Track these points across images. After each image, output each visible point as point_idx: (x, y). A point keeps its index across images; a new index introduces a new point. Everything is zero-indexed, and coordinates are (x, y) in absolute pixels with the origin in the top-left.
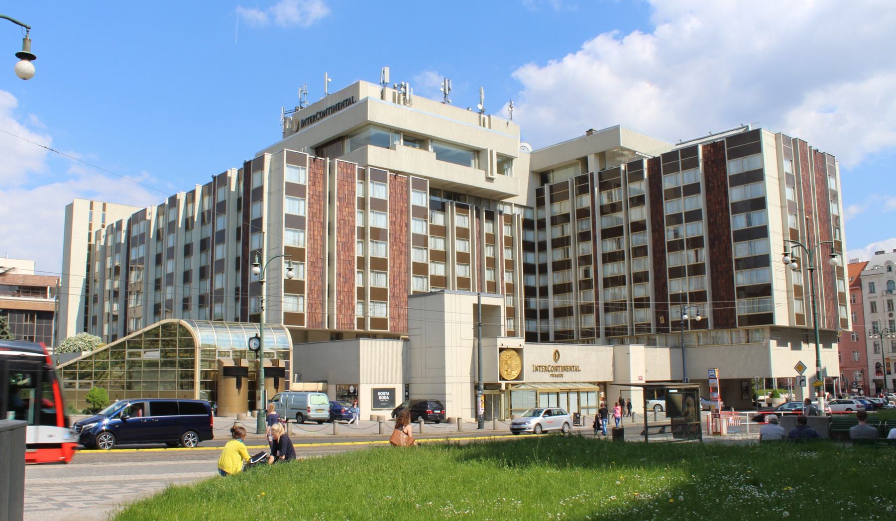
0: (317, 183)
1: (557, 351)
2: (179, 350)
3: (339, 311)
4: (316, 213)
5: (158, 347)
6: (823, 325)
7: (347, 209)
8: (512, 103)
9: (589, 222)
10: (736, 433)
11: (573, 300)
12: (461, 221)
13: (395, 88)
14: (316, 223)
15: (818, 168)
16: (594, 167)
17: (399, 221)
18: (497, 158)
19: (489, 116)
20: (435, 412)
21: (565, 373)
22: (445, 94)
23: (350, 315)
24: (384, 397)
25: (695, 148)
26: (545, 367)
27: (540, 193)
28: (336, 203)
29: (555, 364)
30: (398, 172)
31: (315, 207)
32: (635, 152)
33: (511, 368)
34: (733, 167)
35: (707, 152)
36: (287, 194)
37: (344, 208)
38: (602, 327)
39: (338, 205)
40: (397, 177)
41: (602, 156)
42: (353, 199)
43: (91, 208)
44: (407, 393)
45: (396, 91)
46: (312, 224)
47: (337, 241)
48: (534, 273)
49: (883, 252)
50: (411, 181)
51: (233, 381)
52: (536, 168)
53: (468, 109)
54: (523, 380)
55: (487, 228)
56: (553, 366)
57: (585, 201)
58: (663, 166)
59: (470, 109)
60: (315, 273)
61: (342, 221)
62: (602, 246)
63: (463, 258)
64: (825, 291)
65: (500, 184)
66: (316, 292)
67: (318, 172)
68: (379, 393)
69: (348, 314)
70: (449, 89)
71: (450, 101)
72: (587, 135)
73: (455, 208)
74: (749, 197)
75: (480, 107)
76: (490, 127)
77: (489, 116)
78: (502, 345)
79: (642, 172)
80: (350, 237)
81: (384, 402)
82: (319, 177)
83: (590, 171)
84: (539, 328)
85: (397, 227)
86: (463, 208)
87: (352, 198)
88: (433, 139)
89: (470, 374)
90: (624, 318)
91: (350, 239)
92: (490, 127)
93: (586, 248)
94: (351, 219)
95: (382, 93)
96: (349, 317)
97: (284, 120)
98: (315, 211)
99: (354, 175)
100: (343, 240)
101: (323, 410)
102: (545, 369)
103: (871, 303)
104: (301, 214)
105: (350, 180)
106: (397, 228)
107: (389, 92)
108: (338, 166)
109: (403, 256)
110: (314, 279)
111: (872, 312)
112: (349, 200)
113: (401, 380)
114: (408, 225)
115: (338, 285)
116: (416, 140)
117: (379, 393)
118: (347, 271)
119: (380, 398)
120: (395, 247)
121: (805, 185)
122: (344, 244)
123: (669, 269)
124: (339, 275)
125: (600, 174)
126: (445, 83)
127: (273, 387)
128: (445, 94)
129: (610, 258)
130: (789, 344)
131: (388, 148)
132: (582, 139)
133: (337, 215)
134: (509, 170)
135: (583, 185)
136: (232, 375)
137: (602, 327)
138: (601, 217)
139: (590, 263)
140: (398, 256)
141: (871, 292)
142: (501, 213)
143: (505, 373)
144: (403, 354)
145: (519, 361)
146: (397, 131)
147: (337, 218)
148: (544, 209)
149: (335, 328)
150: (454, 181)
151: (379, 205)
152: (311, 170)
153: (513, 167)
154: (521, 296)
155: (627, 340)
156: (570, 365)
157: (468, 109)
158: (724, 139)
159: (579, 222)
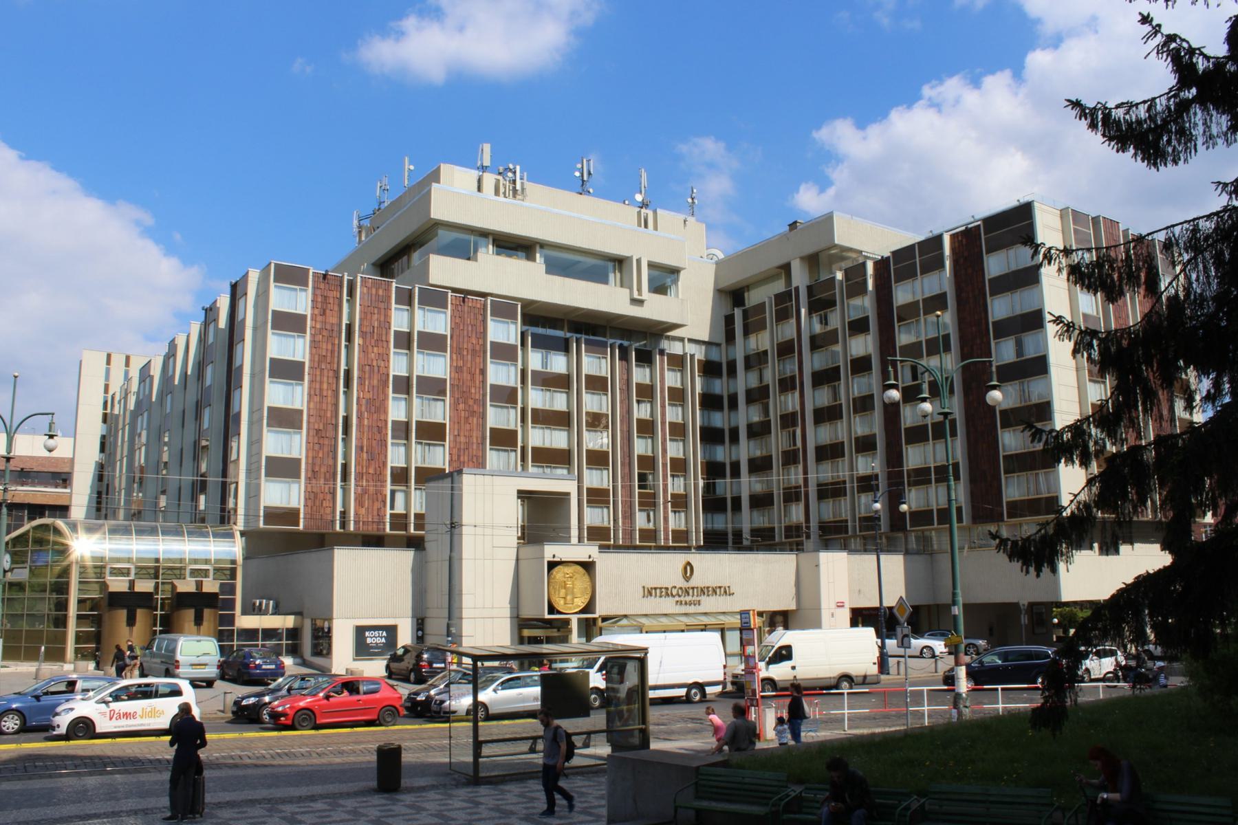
0: (328, 311)
1: (689, 564)
3: (359, 502)
4: (323, 356)
5: (27, 562)
7: (375, 349)
8: (695, 191)
9: (794, 362)
10: (811, 731)
11: (779, 479)
12: (593, 365)
13: (500, 174)
14: (325, 371)
16: (800, 278)
17: (469, 366)
18: (649, 269)
19: (655, 212)
20: (435, 665)
21: (703, 599)
22: (583, 181)
23: (379, 510)
24: (373, 639)
25: (938, 239)
26: (667, 589)
27: (729, 320)
28: (357, 340)
29: (684, 584)
31: (324, 347)
32: (862, 251)
33: (573, 593)
34: (995, 265)
35: (957, 245)
36: (273, 328)
37: (370, 348)
38: (814, 524)
39: (361, 343)
40: (466, 300)
41: (813, 261)
42: (387, 334)
43: (108, 362)
44: (420, 633)
45: (500, 178)
46: (318, 373)
47: (358, 398)
48: (722, 442)
50: (489, 306)
51: (123, 614)
52: (723, 285)
53: (624, 203)
54: (594, 613)
55: (640, 375)
56: (681, 588)
57: (788, 331)
58: (894, 269)
59: (627, 202)
60: (321, 446)
61: (367, 367)
63: (596, 421)
65: (655, 309)
66: (322, 476)
67: (331, 294)
68: (367, 634)
69: (375, 508)
70: (589, 174)
71: (591, 191)
72: (791, 230)
73: (583, 345)
74: (1018, 312)
75: (639, 198)
76: (656, 228)
77: (655, 212)
78: (554, 556)
79: (865, 282)
80: (381, 391)
81: (377, 646)
83: (794, 284)
84: (730, 526)
85: (465, 374)
86: (597, 348)
87: (384, 332)
88: (543, 245)
89: (510, 603)
90: (841, 509)
92: (656, 228)
93: (791, 402)
94: (382, 364)
95: (480, 181)
96: (375, 513)
97: (357, 230)
98: (324, 354)
99: (389, 297)
100: (368, 396)
101: (205, 665)
102: (666, 592)
104: (298, 358)
105: (382, 306)
106: (466, 376)
107: (489, 179)
108: (362, 285)
109: (475, 419)
110: (321, 455)
112: (380, 335)
113: (410, 613)
114: (483, 372)
115: (357, 463)
117: (367, 634)
118: (374, 442)
119: (369, 641)
120: (462, 406)
122: (369, 401)
123: (906, 429)
124: (360, 449)
125: (810, 288)
126: (583, 165)
127: (193, 623)
128: (583, 181)
129: (826, 415)
130: (1096, 545)
131: (469, 259)
132: (782, 238)
133: (359, 358)
134: (673, 287)
135: (784, 305)
136: (122, 607)
137: (814, 524)
138: (812, 354)
139: (794, 424)
142: (662, 352)
143: (562, 602)
144: (413, 570)
145: (587, 584)
146: (484, 234)
147: (359, 364)
148: (734, 344)
149: (352, 529)
151: (432, 342)
152: (318, 292)
153: (680, 283)
154: (696, 478)
155: (808, 544)
156: (714, 586)
157: (624, 203)
158: (979, 223)
159: (781, 362)
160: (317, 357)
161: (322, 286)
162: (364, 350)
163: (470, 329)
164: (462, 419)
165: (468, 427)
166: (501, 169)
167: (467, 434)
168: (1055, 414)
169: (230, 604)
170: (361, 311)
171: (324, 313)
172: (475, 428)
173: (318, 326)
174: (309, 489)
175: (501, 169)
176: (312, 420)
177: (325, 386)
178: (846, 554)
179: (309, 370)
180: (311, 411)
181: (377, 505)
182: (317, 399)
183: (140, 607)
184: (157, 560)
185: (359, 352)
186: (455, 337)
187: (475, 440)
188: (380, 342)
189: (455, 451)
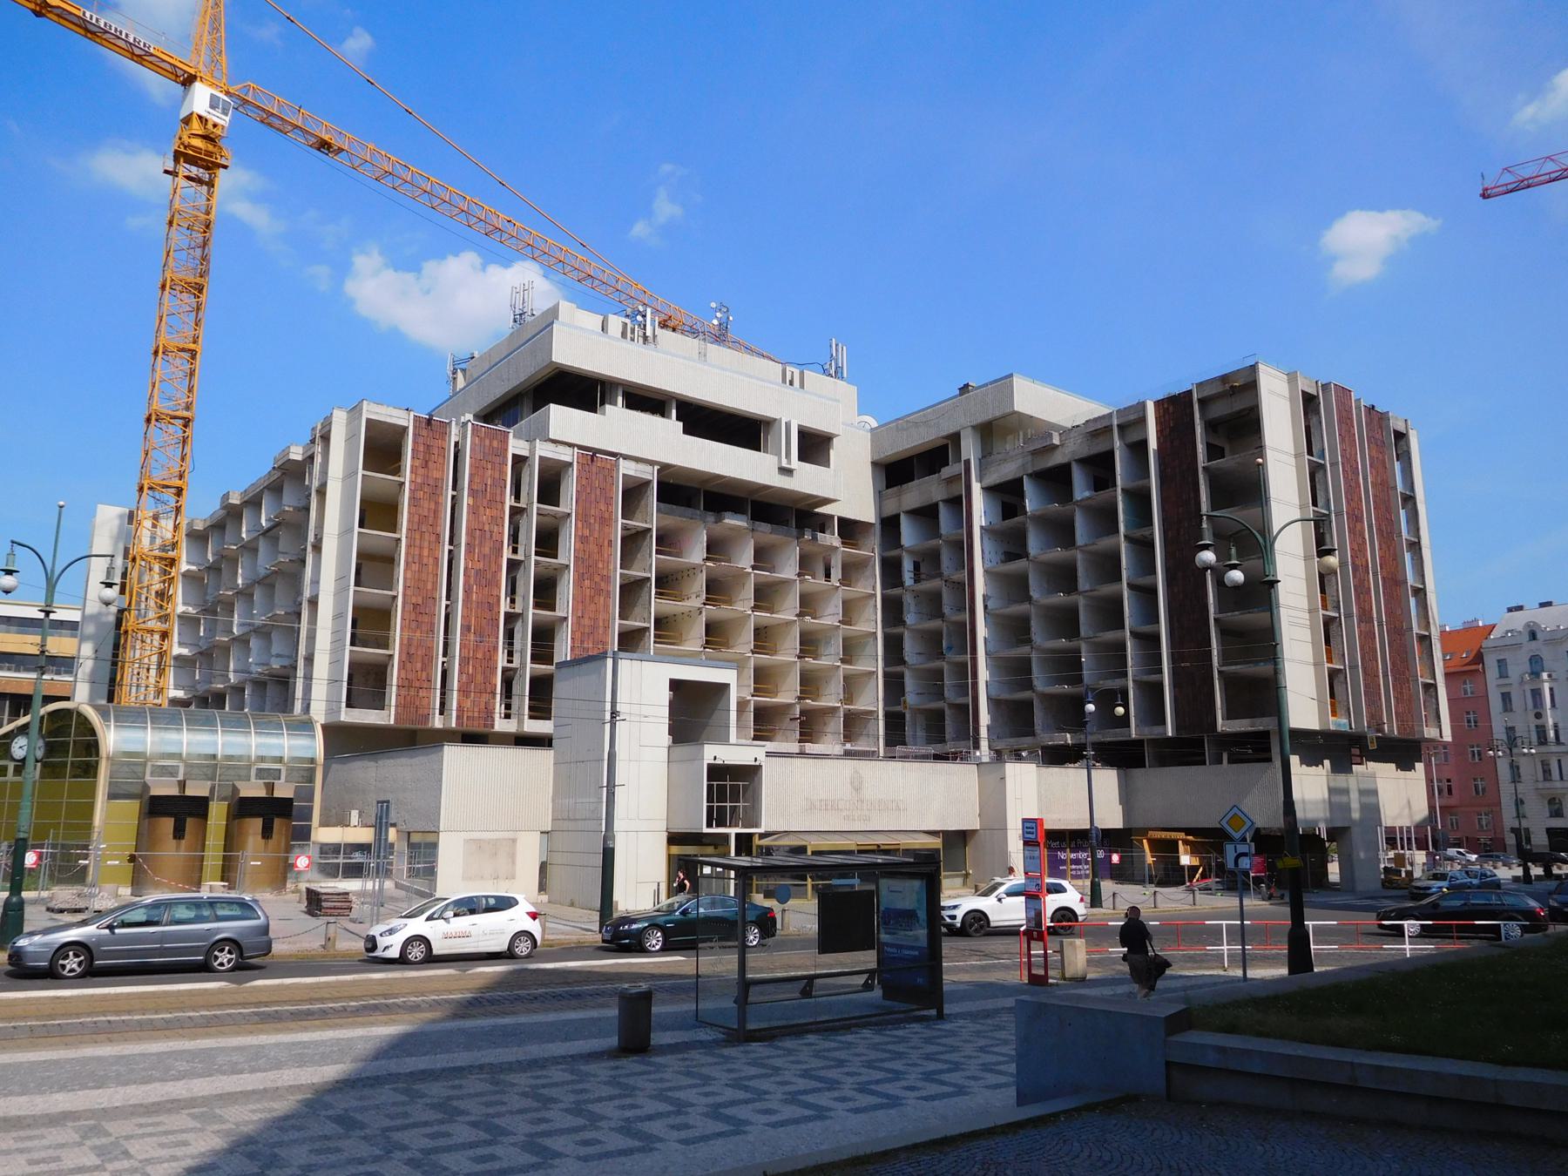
2: (72, 763)
6: (1392, 728)
13: (627, 316)
14: (427, 535)
15: (1376, 439)
30: (596, 451)
31: (426, 505)
37: (482, 508)
45: (627, 321)
46: (418, 537)
49: (1520, 608)
52: (881, 456)
62: (571, 445)
64: (1393, 664)
65: (807, 480)
66: (420, 659)
76: (802, 386)
78: (715, 758)
82: (436, 453)
87: (498, 492)
91: (493, 565)
92: (802, 386)
100: (480, 566)
103: (1503, 694)
105: (497, 460)
106: (593, 547)
107: (615, 322)
108: (472, 434)
111: (1506, 710)
116: (645, 401)
120: (587, 582)
121: (1348, 468)
127: (260, 836)
133: (468, 521)
140: (592, 598)
141: (1501, 677)
147: (467, 527)
150: (722, 474)
152: (421, 440)
160: (417, 517)
161: (424, 433)
162: (473, 511)
163: (598, 492)
164: (588, 599)
165: (593, 606)
166: (629, 311)
167: (592, 615)
168: (1282, 610)
169: (307, 814)
170: (471, 466)
171: (426, 465)
172: (602, 609)
173: (419, 480)
174: (403, 676)
175: (629, 311)
176: (409, 592)
177: (426, 553)
178: (1034, 766)
179: (407, 533)
180: (408, 581)
181: (485, 697)
182: (415, 567)
183: (191, 815)
184: (214, 757)
185: (468, 513)
186: (580, 501)
187: (601, 624)
188: (493, 503)
189: (578, 635)
